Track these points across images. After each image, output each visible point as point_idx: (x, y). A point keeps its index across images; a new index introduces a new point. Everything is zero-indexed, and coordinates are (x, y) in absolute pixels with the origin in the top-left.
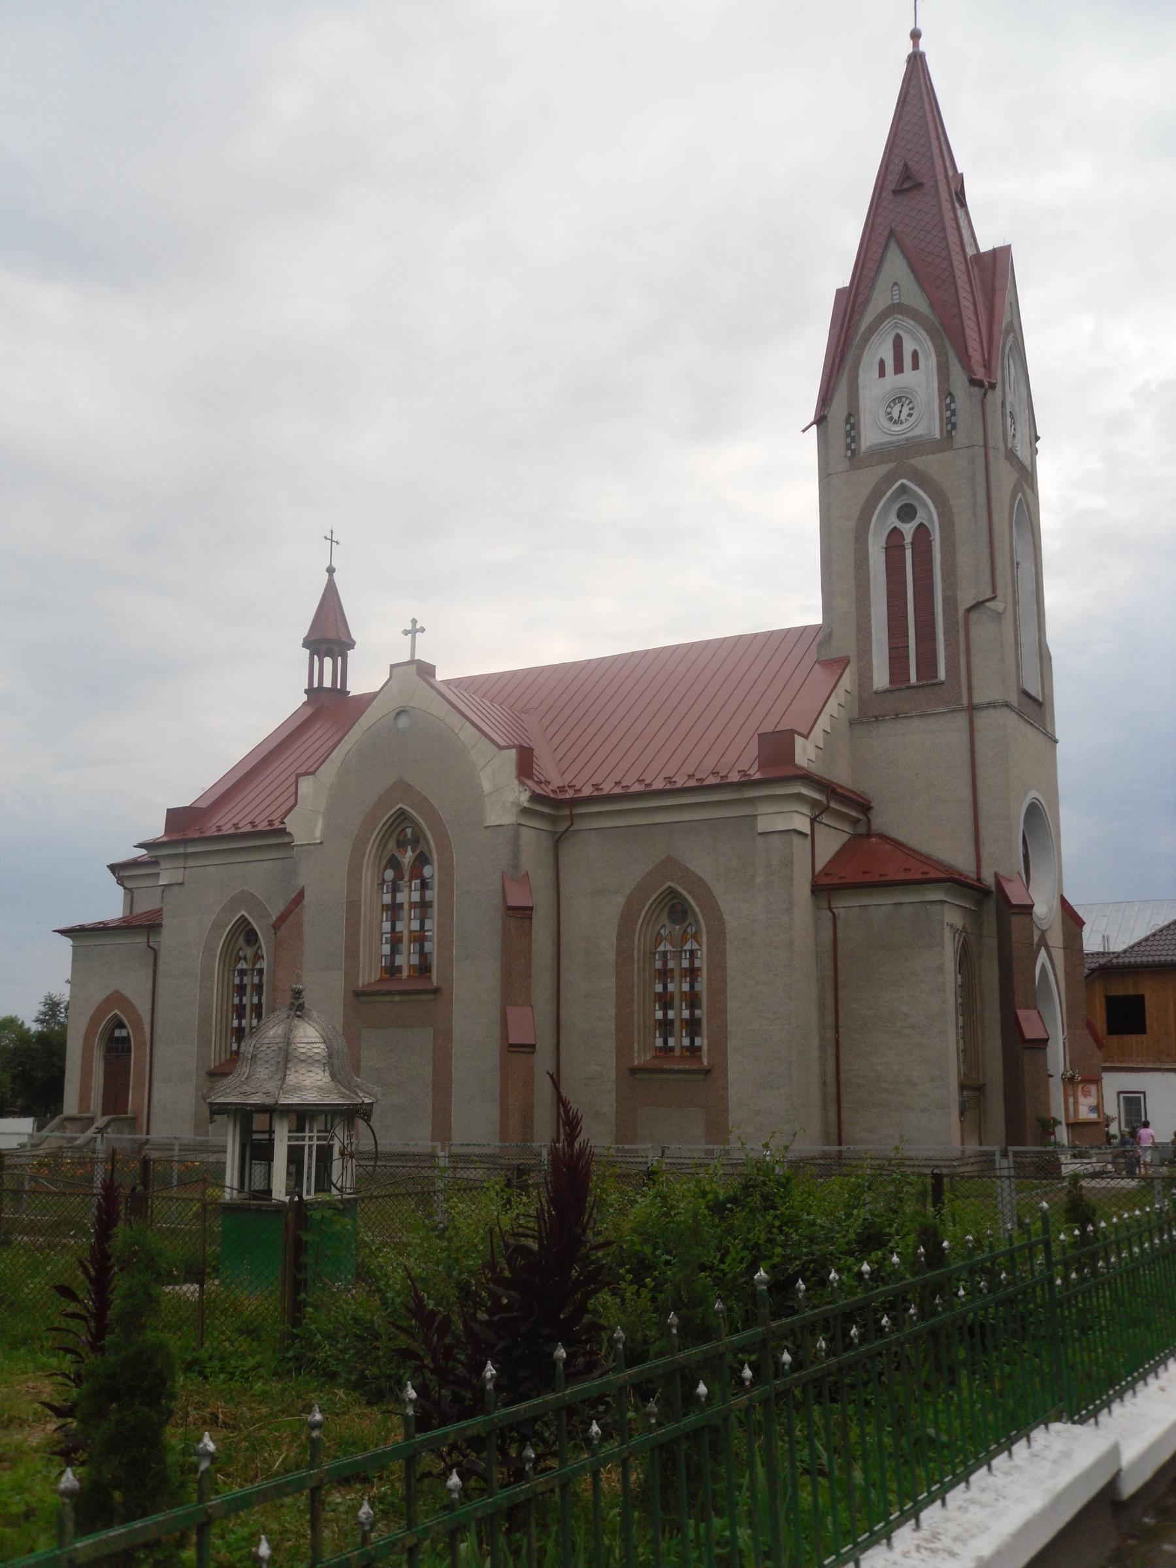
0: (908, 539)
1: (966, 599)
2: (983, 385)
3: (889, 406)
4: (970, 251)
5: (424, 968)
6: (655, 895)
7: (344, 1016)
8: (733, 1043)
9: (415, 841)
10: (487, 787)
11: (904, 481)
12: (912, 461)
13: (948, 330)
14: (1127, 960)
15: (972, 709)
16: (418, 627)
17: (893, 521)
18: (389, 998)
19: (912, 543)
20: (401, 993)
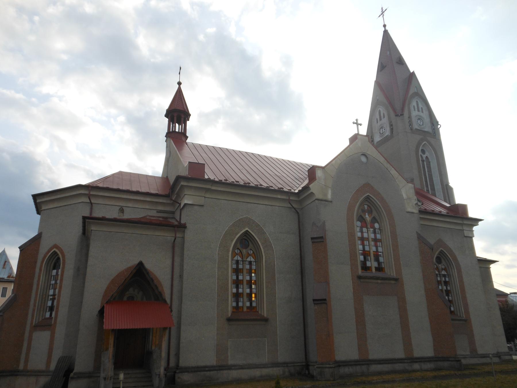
5: (379, 269)
7: (354, 289)
10: (405, 196)
16: (355, 121)
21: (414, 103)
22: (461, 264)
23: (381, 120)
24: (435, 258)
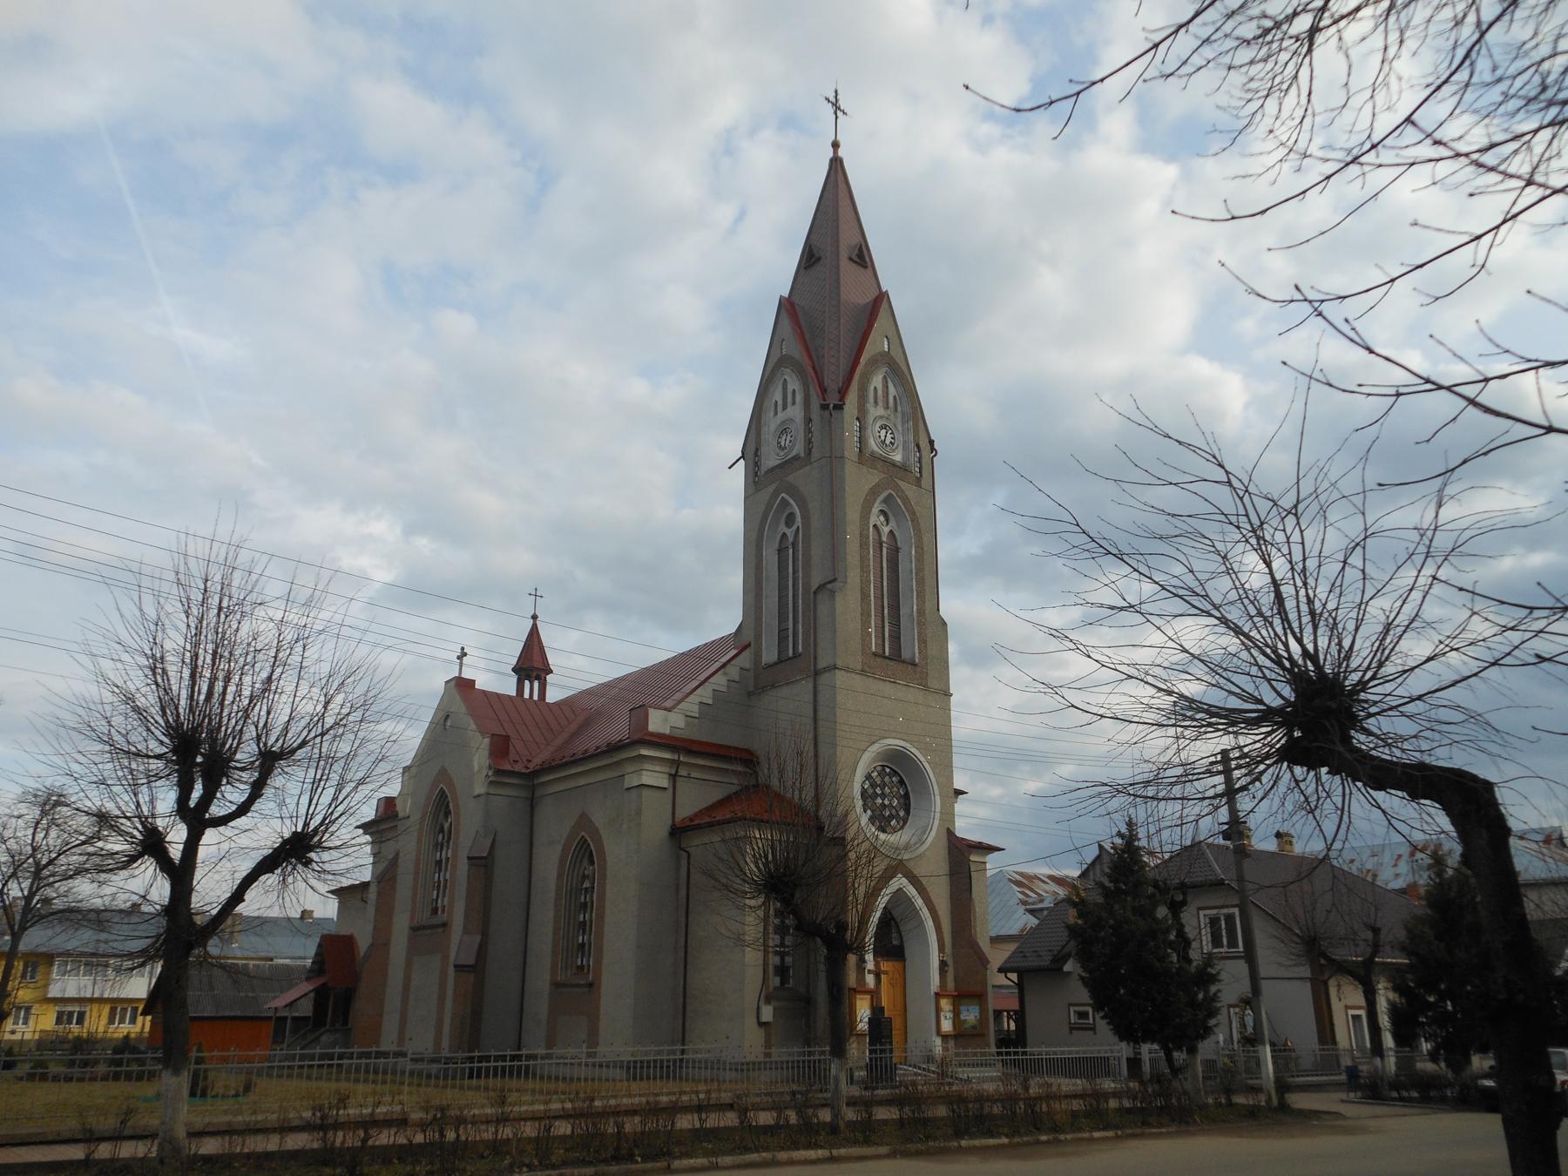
10: (476, 768)
17: (783, 528)
21: (877, 381)
23: (785, 407)
24: (875, 748)
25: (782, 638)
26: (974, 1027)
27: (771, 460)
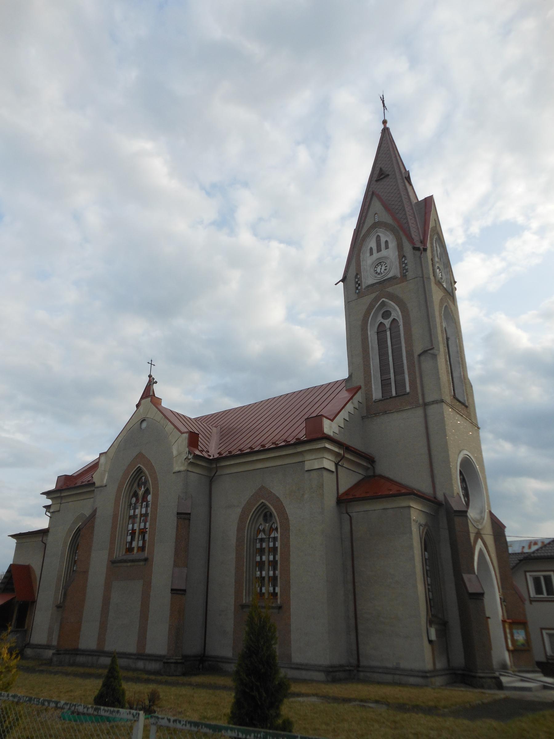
0: (388, 326)
1: (418, 349)
2: (420, 250)
3: (376, 267)
4: (415, 201)
6: (255, 508)
8: (294, 590)
9: (145, 483)
10: (175, 453)
11: (384, 299)
12: (387, 290)
13: (400, 230)
14: (539, 554)
15: (426, 405)
17: (380, 319)
18: (125, 564)
19: (390, 329)
20: (131, 562)
22: (290, 518)
25: (385, 384)
26: (523, 645)
27: (369, 279)
